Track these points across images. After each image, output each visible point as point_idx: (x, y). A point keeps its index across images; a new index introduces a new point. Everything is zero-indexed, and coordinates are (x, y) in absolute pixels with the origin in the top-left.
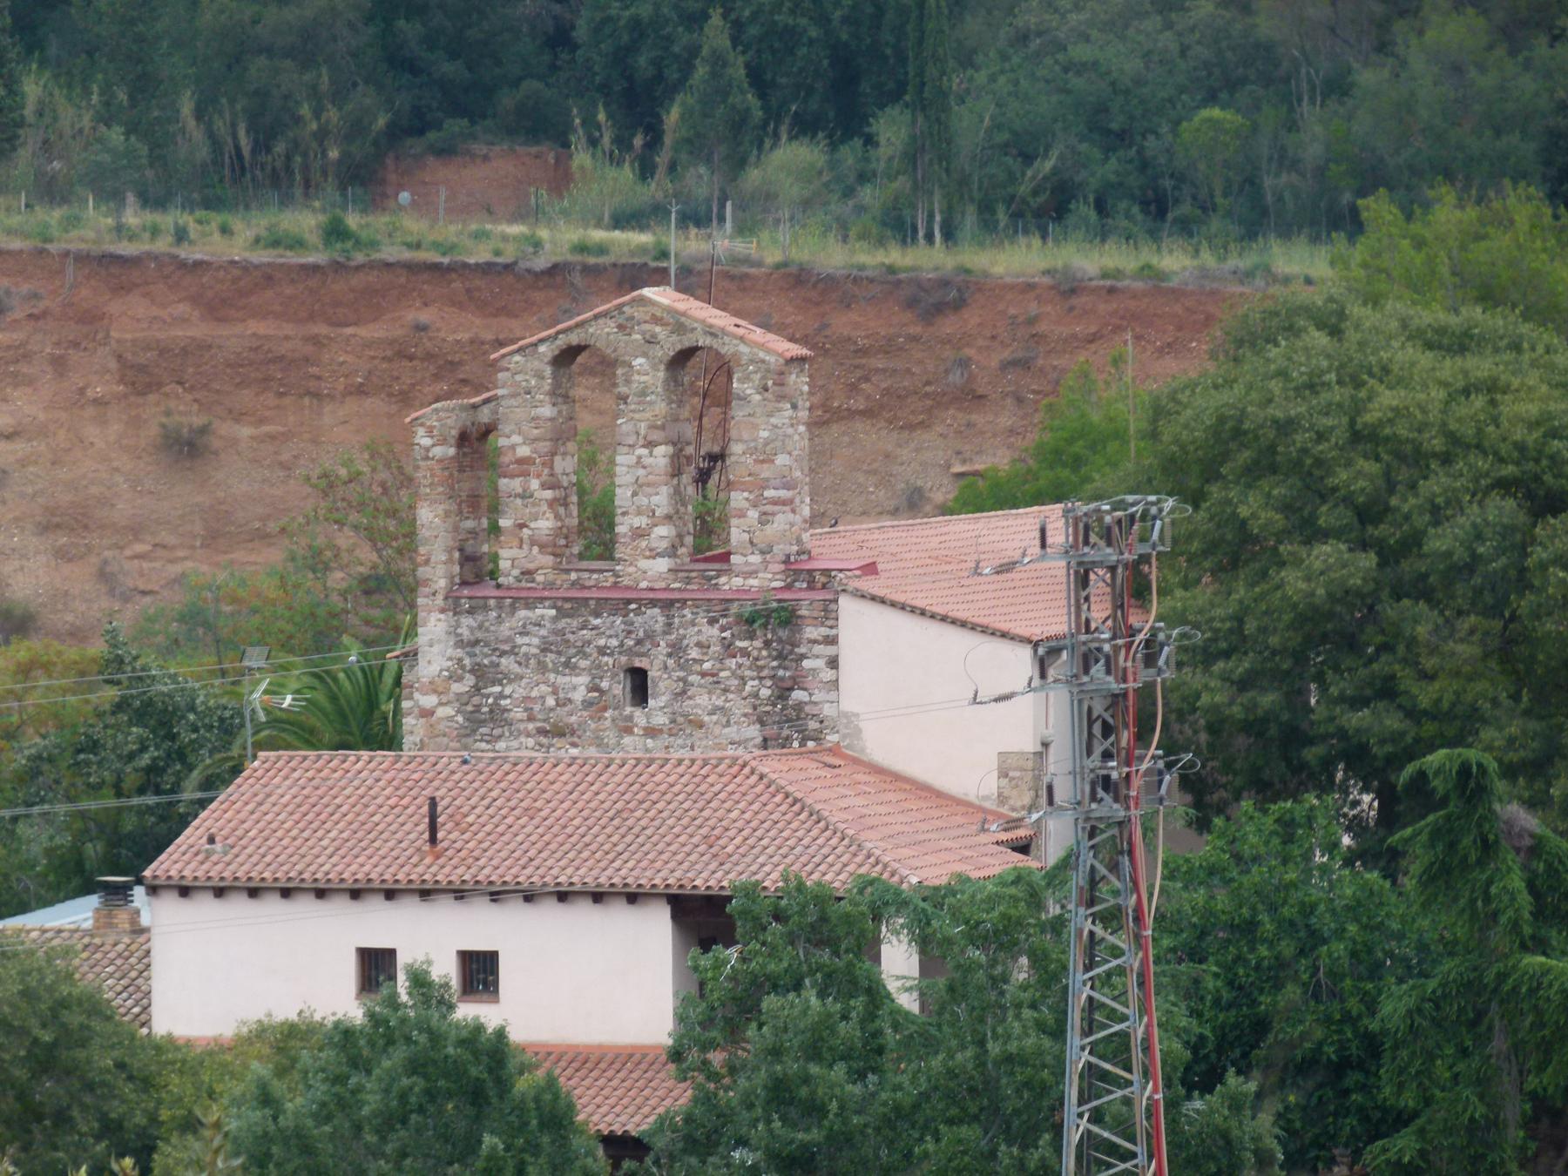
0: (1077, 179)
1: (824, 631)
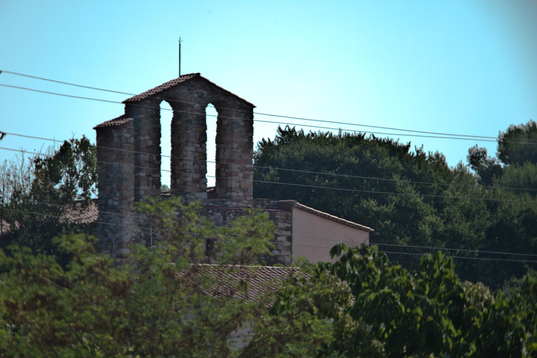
0: (355, 322)
1: (286, 225)
